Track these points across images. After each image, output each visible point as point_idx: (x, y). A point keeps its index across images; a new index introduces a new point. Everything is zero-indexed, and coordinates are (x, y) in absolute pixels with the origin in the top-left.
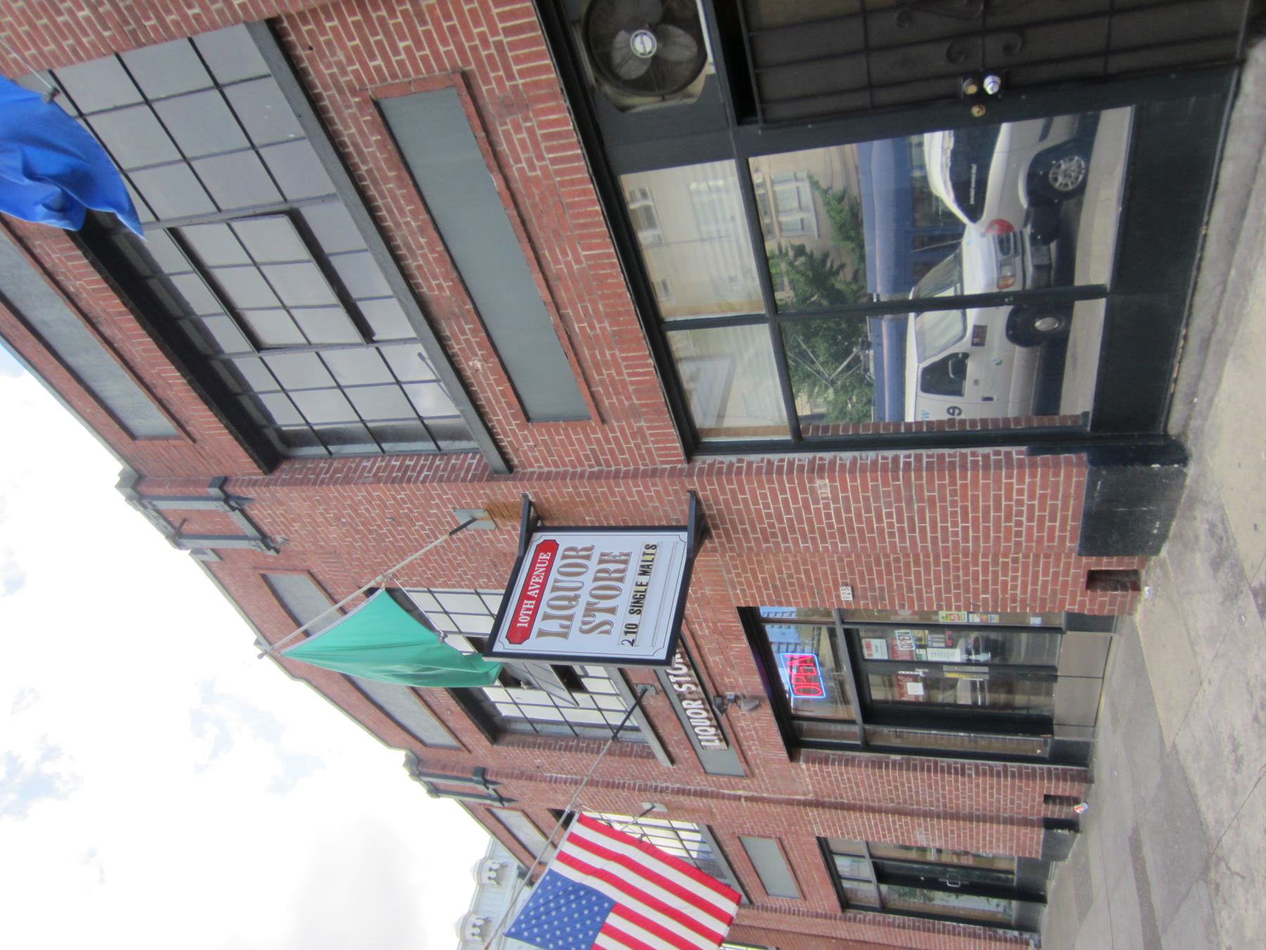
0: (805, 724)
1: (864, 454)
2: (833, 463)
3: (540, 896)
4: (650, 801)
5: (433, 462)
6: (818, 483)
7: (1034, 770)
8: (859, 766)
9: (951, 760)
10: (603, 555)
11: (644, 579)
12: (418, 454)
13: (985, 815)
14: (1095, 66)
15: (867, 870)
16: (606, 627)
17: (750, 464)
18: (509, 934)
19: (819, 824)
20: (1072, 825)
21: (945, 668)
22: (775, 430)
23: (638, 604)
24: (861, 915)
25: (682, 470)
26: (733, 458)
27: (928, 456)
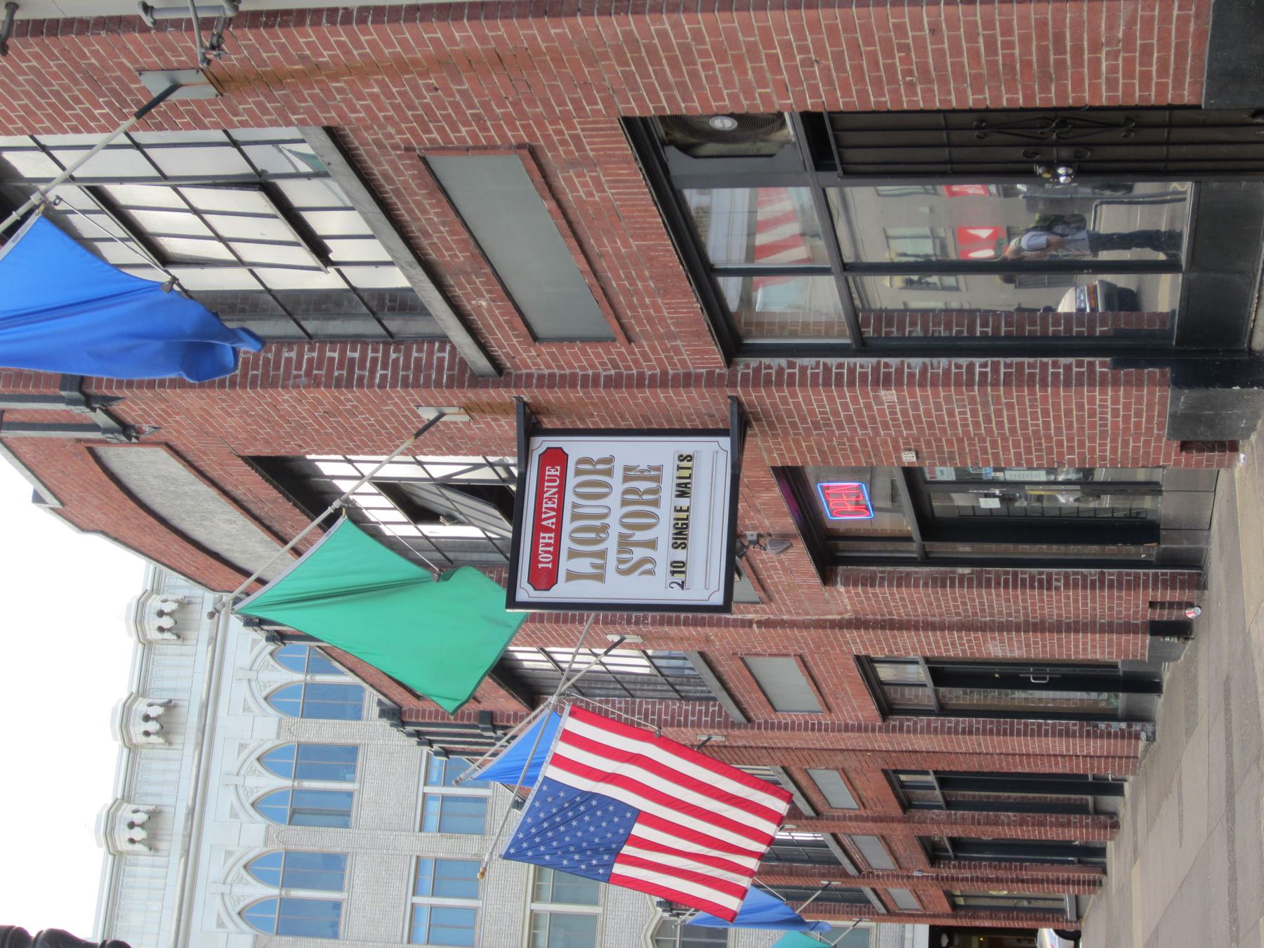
0: (841, 544)
1: (935, 360)
2: (900, 371)
3: (540, 810)
4: (618, 633)
5: (386, 355)
6: (883, 393)
7: (1137, 576)
8: (916, 586)
9: (1034, 570)
10: (627, 469)
11: (684, 502)
12: (356, 339)
13: (1077, 623)
14: (1161, 166)
15: (919, 673)
16: (648, 566)
17: (803, 369)
18: (507, 856)
19: (860, 642)
20: (1182, 630)
21: (1027, 487)
22: (829, 326)
23: (681, 535)
24: (909, 722)
25: (721, 376)
26: (783, 362)
27: (1006, 366)
